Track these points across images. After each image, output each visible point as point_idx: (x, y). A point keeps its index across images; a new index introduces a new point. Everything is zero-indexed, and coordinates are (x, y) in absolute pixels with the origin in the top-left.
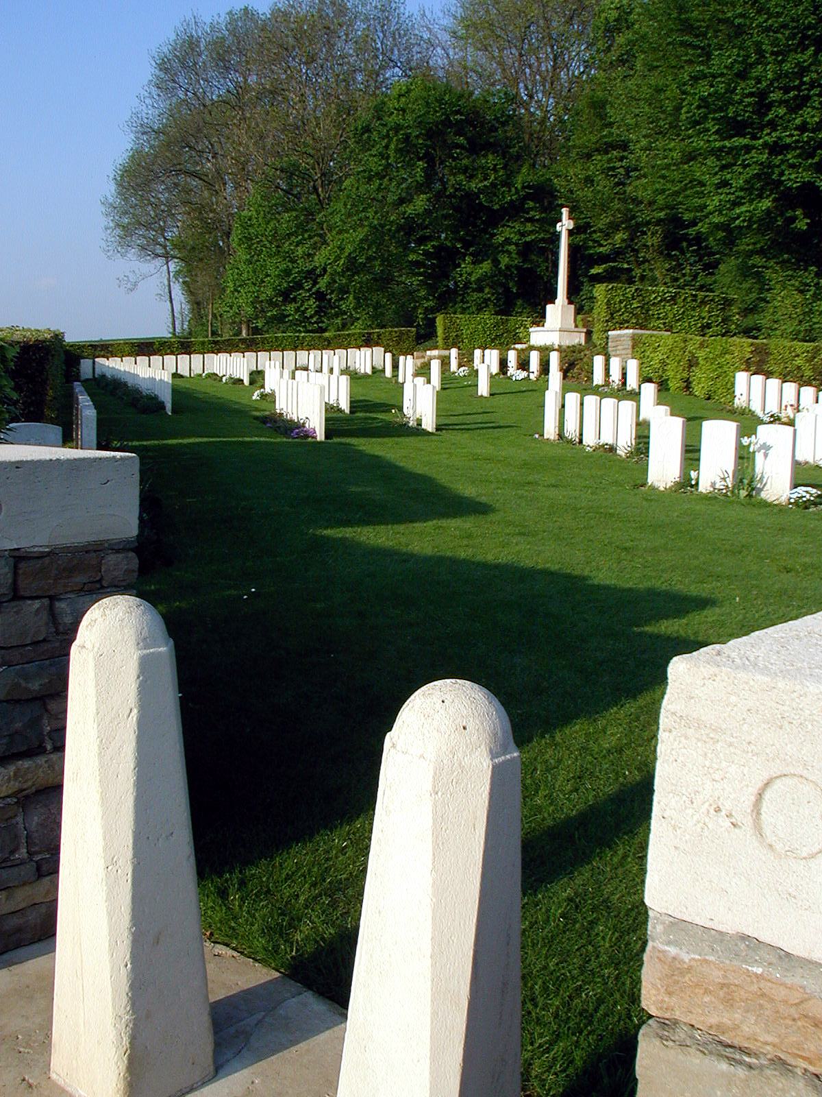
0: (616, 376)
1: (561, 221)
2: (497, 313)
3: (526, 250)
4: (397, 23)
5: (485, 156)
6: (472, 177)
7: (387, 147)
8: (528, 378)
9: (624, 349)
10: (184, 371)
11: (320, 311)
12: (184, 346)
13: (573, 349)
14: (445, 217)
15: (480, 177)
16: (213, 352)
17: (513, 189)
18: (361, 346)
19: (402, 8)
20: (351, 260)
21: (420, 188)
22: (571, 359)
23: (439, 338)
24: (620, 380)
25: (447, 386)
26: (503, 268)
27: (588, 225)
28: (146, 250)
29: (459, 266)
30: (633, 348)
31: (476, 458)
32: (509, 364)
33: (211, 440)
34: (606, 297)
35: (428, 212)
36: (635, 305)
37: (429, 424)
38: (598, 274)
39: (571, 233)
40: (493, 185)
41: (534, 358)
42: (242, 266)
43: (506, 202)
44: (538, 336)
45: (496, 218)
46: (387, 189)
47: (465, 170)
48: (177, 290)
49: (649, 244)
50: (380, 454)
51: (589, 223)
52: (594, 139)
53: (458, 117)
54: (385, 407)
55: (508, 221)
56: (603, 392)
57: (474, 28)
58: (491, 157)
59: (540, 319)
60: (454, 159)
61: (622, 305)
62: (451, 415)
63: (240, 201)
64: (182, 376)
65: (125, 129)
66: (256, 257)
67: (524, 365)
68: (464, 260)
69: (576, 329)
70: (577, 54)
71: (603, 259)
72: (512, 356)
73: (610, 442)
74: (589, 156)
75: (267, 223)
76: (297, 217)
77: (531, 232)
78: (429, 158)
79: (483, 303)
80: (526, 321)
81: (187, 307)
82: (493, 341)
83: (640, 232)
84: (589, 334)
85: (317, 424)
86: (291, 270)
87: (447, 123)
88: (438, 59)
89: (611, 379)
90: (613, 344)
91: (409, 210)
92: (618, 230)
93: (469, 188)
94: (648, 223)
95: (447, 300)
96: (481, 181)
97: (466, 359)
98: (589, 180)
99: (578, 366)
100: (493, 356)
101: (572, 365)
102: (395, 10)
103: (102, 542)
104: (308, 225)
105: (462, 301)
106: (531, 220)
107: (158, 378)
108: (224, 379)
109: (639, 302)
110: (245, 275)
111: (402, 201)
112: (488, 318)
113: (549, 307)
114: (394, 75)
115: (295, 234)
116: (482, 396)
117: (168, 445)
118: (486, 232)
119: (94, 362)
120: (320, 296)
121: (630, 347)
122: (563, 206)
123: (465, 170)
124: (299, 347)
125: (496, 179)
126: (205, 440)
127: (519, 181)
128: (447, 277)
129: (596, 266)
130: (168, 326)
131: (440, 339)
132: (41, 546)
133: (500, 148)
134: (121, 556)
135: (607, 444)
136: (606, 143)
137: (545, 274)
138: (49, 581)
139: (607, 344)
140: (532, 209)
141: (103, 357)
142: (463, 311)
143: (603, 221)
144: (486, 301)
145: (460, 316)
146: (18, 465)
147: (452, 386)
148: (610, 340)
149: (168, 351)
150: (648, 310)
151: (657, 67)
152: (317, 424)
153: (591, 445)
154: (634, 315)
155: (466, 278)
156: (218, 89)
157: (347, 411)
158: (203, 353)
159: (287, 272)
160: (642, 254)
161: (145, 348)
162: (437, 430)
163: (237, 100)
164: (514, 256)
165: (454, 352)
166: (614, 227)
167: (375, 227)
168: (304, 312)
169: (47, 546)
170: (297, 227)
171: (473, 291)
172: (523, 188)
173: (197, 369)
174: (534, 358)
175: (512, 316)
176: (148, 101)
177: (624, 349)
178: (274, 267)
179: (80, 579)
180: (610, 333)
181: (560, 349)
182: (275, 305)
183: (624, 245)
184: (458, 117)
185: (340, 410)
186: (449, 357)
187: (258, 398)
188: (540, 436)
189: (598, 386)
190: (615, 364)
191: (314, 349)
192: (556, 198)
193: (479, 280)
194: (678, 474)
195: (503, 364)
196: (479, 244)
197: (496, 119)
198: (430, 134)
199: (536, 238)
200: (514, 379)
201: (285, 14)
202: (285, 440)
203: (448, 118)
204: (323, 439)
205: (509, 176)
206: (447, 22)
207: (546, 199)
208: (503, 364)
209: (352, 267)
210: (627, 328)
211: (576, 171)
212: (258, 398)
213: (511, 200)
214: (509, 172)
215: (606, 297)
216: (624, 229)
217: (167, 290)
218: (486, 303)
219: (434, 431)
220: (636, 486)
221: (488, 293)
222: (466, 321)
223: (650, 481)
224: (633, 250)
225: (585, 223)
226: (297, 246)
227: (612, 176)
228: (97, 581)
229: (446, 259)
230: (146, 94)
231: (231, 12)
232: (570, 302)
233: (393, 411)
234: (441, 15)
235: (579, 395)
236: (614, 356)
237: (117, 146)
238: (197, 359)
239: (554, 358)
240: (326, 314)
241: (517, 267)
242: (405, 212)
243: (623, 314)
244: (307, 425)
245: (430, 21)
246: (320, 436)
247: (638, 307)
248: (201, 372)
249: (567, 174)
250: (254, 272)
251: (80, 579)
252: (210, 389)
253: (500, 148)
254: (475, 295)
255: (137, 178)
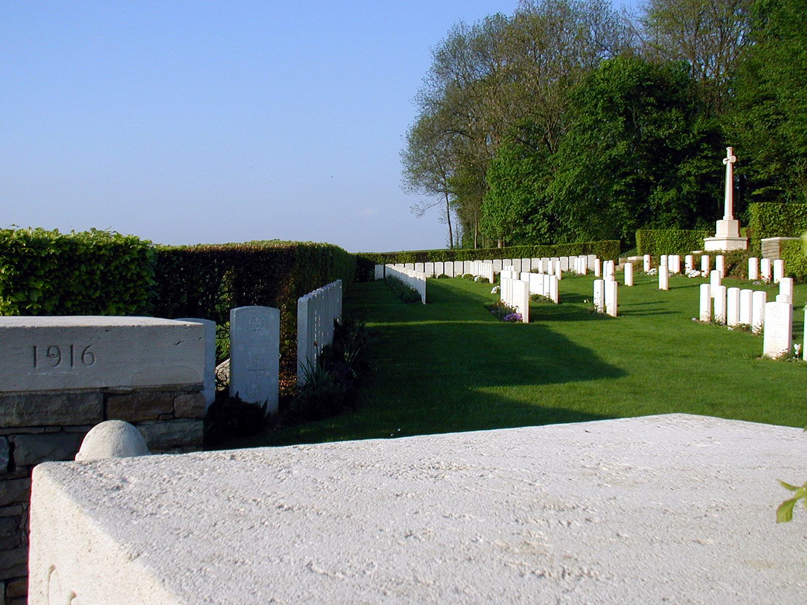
0: (766, 273)
1: (726, 157)
2: (681, 228)
3: (703, 179)
4: (606, 18)
5: (670, 111)
6: (660, 127)
7: (596, 106)
8: (700, 276)
9: (773, 252)
10: (449, 273)
11: (551, 229)
12: (450, 256)
13: (736, 253)
14: (641, 157)
15: (667, 127)
16: (470, 260)
17: (691, 135)
18: (580, 254)
19: (609, 7)
20: (570, 192)
21: (622, 136)
22: (733, 261)
23: (637, 248)
24: (769, 276)
25: (638, 283)
26: (685, 193)
27: (750, 160)
28: (432, 188)
29: (652, 193)
30: (780, 251)
31: (636, 335)
32: (686, 266)
33: (441, 322)
34: (758, 213)
35: (628, 153)
36: (782, 218)
37: (612, 311)
38: (759, 195)
39: (733, 165)
40: (677, 133)
41: (705, 260)
42: (495, 198)
43: (686, 145)
44: (710, 245)
45: (679, 157)
46: (598, 139)
47: (655, 122)
48: (453, 215)
49: (797, 171)
50: (563, 332)
51: (750, 158)
52: (752, 94)
53: (649, 83)
54: (579, 298)
55: (688, 158)
56: (753, 286)
57: (665, 17)
58: (674, 111)
59: (713, 233)
60: (647, 114)
61: (772, 219)
62: (635, 304)
63: (495, 149)
64: (447, 277)
65: (413, 102)
66: (503, 191)
67: (697, 266)
68: (656, 189)
69: (740, 238)
70: (740, 32)
71: (761, 184)
72: (689, 260)
73: (747, 322)
74: (749, 107)
75: (512, 166)
76: (534, 161)
77: (706, 167)
78: (627, 114)
79: (671, 220)
80: (704, 233)
81: (461, 228)
82: (679, 248)
83: (790, 162)
84: (749, 241)
85: (523, 311)
86: (529, 200)
87: (640, 88)
88: (637, 43)
89: (762, 274)
90: (765, 249)
91: (614, 152)
92: (772, 161)
93: (658, 135)
94: (796, 155)
95: (644, 218)
96: (667, 130)
97: (655, 264)
98: (749, 125)
99: (738, 266)
100: (674, 262)
101: (734, 265)
102: (605, 9)
103: (175, 386)
104: (541, 168)
105: (655, 219)
106: (706, 157)
107: (418, 278)
108: (475, 279)
109: (785, 216)
110: (496, 204)
111: (608, 147)
112: (675, 231)
113: (718, 222)
114: (605, 56)
115: (533, 173)
116: (662, 289)
117: (408, 325)
118: (672, 167)
119: (384, 267)
120: (551, 219)
121: (778, 250)
122: (728, 146)
123: (655, 122)
124: (534, 255)
125: (678, 127)
126: (438, 322)
127: (695, 129)
128: (644, 201)
129: (757, 190)
130: (448, 241)
131: (638, 248)
132: (125, 386)
133: (681, 105)
134: (190, 396)
135: (744, 325)
136: (762, 97)
137: (718, 197)
138: (131, 411)
139: (760, 248)
140: (705, 149)
141: (391, 263)
142: (656, 227)
143: (761, 156)
144: (674, 219)
145: (653, 231)
146: (107, 329)
147: (641, 282)
148: (762, 246)
149: (438, 259)
150: (792, 222)
151: (794, 36)
152: (523, 311)
153: (733, 325)
154: (781, 226)
155: (658, 202)
156: (481, 71)
157: (556, 301)
158: (463, 260)
159: (526, 201)
160: (792, 179)
161: (421, 257)
162: (618, 315)
163: (492, 80)
164: (693, 184)
165: (646, 258)
166: (769, 159)
167: (587, 166)
168: (539, 230)
169: (129, 387)
170: (534, 169)
171: (663, 212)
172: (699, 133)
173: (459, 272)
174: (705, 260)
175: (693, 229)
176: (430, 82)
177: (773, 252)
178: (516, 199)
179: (156, 411)
180: (762, 240)
181: (726, 255)
182: (519, 225)
183: (777, 173)
184: (649, 83)
185: (550, 301)
186: (643, 261)
187: (495, 292)
188: (697, 319)
189: (752, 281)
190: (765, 263)
191: (544, 256)
192: (724, 139)
193: (667, 204)
194: (787, 347)
195: (682, 265)
196: (668, 177)
197: (677, 83)
198: (628, 97)
199: (710, 171)
200: (689, 276)
201: (522, 16)
202: (498, 322)
203: (641, 84)
204: (527, 321)
205: (688, 126)
206: (642, 15)
207: (716, 141)
208: (682, 265)
209: (572, 197)
210: (776, 236)
211: (738, 119)
212: (495, 292)
213: (690, 143)
214: (688, 123)
215: (758, 213)
216: (777, 160)
217: (446, 216)
218: (674, 220)
219: (616, 315)
220: (754, 357)
221: (675, 213)
222: (658, 234)
223: (765, 353)
224: (785, 177)
225: (748, 157)
226: (534, 182)
227: (767, 121)
228: (170, 414)
229: (642, 189)
230: (429, 77)
231: (487, 17)
232: (735, 218)
233: (585, 301)
234: (638, 10)
235: (725, 287)
236: (766, 258)
237: (409, 116)
238: (459, 264)
239: (720, 260)
240: (555, 231)
241: (696, 193)
242: (611, 155)
243: (773, 225)
244: (517, 312)
245: (629, 15)
246: (525, 319)
247: (784, 220)
248: (461, 274)
249: (733, 122)
250: (503, 202)
251: (156, 411)
252: (465, 287)
253: (681, 105)
254: (665, 215)
255: (424, 135)
